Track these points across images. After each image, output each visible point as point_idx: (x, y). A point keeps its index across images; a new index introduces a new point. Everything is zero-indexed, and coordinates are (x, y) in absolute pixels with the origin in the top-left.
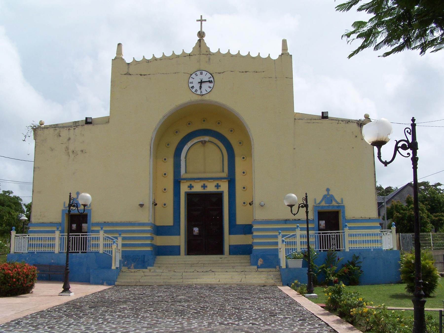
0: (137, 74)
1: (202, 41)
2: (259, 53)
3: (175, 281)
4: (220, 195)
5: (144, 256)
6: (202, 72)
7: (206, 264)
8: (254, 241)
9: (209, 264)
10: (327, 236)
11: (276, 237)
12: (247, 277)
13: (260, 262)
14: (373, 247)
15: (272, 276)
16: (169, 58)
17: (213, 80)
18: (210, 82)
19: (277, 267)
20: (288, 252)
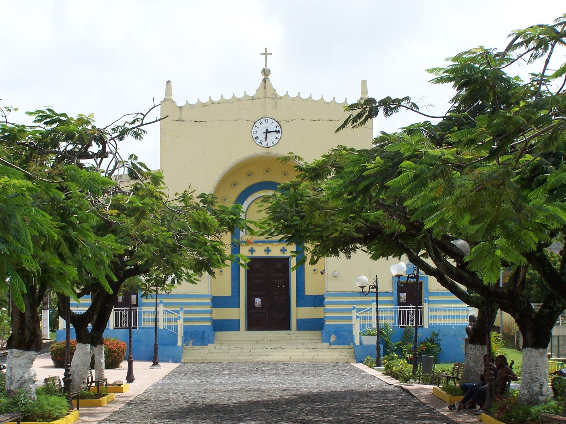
0: (191, 121)
1: (267, 80)
2: (334, 97)
3: (244, 358)
4: (286, 261)
5: (204, 332)
6: (267, 120)
7: (272, 340)
8: (326, 315)
9: (275, 340)
10: (405, 311)
11: (178, 312)
12: (319, 354)
13: (333, 338)
14: (454, 324)
15: (345, 354)
16: (229, 102)
17: (280, 130)
18: (277, 132)
19: (352, 344)
20: (363, 328)
